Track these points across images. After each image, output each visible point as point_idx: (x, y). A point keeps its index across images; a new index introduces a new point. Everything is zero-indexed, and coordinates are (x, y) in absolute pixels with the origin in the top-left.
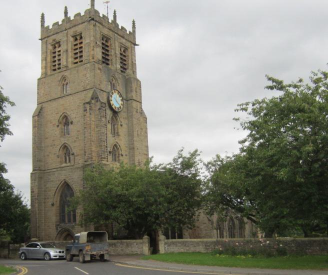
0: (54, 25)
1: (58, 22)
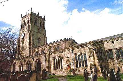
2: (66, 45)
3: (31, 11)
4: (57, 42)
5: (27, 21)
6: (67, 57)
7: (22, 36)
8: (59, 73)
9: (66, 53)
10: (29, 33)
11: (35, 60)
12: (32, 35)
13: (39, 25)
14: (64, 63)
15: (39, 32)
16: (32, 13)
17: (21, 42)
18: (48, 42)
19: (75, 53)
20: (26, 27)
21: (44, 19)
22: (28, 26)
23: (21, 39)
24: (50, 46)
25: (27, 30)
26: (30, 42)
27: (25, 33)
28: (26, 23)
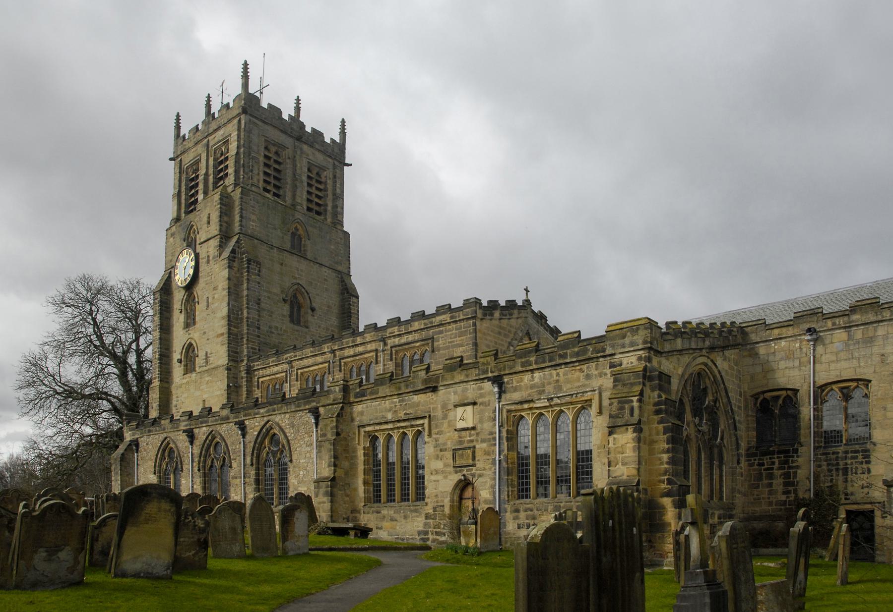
2: (476, 344)
3: (245, 85)
4: (416, 325)
5: (215, 167)
6: (458, 429)
7: (182, 276)
8: (397, 525)
9: (454, 399)
10: (226, 253)
11: (252, 433)
12: (242, 262)
13: (302, 197)
14: (439, 465)
15: (297, 247)
16: (249, 104)
17: (178, 319)
18: (363, 322)
19: (516, 396)
20: (209, 209)
21: (336, 153)
22: (217, 197)
23: (178, 296)
24: (369, 347)
25: (214, 229)
26: (233, 319)
27: (202, 251)
28: (211, 179)
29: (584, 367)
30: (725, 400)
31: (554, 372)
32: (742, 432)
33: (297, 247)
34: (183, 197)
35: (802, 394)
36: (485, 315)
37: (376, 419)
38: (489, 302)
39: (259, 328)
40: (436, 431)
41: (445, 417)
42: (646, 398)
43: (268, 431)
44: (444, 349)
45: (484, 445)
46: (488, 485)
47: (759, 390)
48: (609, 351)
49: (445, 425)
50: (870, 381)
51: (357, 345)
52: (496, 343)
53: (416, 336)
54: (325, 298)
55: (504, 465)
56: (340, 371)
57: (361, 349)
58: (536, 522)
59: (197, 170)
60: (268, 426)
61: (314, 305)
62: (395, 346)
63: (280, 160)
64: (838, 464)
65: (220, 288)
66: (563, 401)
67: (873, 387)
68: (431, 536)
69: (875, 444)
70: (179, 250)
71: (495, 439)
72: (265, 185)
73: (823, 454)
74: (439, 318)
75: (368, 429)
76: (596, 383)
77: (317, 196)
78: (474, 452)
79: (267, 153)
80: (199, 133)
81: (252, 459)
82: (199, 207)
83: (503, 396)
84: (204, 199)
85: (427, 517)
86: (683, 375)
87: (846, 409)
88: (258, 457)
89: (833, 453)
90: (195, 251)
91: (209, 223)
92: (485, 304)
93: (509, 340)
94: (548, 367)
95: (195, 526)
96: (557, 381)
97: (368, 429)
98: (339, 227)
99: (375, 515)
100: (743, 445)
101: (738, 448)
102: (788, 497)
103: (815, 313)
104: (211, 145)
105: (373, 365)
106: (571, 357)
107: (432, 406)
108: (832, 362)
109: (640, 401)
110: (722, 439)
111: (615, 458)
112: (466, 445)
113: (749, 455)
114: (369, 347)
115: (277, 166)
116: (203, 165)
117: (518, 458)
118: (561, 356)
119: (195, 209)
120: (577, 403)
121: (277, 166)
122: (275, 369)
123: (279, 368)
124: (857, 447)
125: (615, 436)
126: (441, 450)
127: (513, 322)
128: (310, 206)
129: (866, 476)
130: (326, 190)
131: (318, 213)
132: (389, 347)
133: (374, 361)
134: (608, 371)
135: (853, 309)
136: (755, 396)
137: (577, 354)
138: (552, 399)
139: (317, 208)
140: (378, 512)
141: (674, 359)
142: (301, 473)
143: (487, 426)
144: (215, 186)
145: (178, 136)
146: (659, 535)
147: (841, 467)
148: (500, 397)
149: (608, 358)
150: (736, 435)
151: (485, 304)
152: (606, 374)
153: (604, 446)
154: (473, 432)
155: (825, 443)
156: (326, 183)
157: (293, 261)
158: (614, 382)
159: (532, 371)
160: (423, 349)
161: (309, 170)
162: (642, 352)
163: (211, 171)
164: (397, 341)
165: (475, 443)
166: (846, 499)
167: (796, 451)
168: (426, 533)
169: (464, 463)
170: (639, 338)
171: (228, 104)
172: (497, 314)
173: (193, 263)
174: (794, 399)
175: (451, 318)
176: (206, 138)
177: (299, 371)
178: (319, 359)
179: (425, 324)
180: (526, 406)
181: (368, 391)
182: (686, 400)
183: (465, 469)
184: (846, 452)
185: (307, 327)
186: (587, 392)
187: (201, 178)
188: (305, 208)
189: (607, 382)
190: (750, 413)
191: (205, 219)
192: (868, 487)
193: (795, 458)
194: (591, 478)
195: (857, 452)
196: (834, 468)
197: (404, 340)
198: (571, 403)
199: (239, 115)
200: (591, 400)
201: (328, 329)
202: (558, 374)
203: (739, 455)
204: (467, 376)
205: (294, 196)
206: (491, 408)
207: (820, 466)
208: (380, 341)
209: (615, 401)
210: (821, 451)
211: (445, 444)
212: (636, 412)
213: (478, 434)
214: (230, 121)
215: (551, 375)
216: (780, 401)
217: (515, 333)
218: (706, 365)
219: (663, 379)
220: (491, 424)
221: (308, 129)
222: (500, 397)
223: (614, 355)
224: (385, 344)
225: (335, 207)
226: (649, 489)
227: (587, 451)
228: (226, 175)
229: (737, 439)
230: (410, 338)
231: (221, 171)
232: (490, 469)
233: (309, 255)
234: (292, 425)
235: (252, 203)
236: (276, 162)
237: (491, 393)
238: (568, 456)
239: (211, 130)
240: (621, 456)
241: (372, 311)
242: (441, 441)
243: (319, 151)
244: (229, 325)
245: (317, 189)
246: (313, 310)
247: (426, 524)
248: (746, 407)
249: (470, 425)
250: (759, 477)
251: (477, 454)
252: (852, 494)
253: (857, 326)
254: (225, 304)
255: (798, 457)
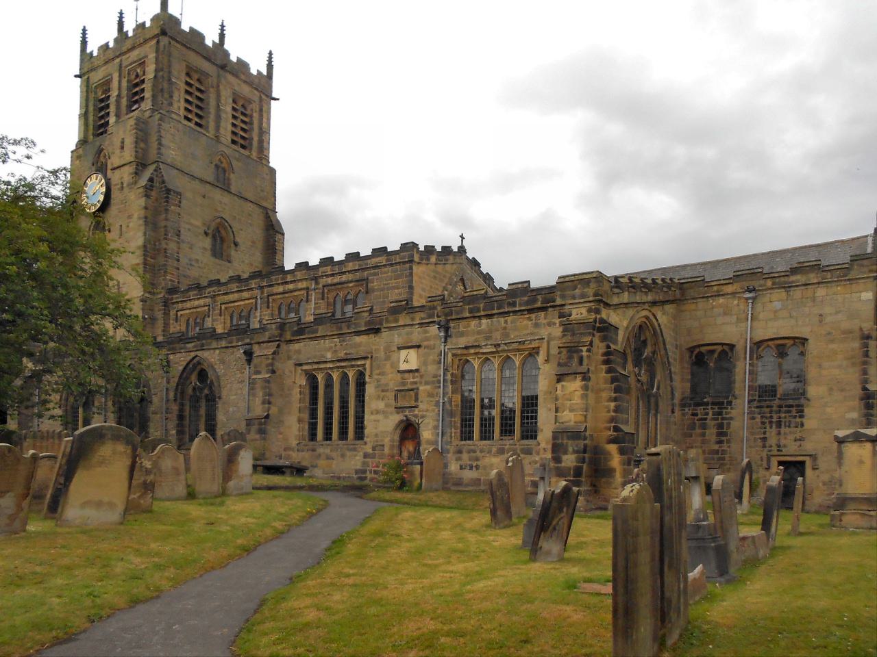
0: (101, 48)
1: (107, 44)
5: (129, 89)
10: (143, 181)
14: (381, 405)
15: (222, 180)
19: (463, 341)
21: (263, 86)
22: (132, 122)
24: (300, 285)
25: (128, 155)
28: (124, 102)
29: (533, 316)
30: (663, 352)
31: (502, 320)
32: (677, 383)
33: (222, 180)
34: (91, 118)
35: (739, 347)
36: (422, 259)
37: (315, 358)
38: (426, 247)
39: (178, 260)
40: (378, 372)
41: (388, 358)
42: (594, 349)
43: (195, 366)
44: (378, 290)
45: (428, 387)
46: (430, 427)
47: (695, 344)
48: (559, 302)
49: (388, 366)
50: (807, 340)
51: (287, 283)
52: (431, 287)
53: (350, 277)
54: (249, 234)
55: (448, 406)
56: (268, 307)
57: (291, 286)
58: (479, 463)
59: (109, 90)
60: (195, 361)
61: (238, 239)
62: (328, 286)
63: (203, 88)
64: (771, 417)
65: (136, 216)
66: (511, 348)
67: (812, 346)
68: (369, 475)
69: (808, 400)
70: (87, 173)
71: (439, 382)
72: (186, 113)
73: (757, 407)
74: (374, 260)
75: (305, 367)
76: (544, 332)
77: (242, 129)
78: (417, 395)
79: (188, 80)
80: (110, 52)
81: (176, 394)
82: (110, 129)
83: (449, 340)
84: (116, 122)
85: (366, 456)
86: (627, 328)
87: (780, 365)
88: (183, 393)
89: (767, 407)
90: (105, 177)
91: (122, 148)
92: (422, 248)
93: (444, 285)
94: (497, 314)
95: (142, 467)
96: (505, 328)
97: (305, 367)
98: (264, 162)
99: (310, 452)
100: (678, 395)
101: (673, 399)
102: (720, 447)
103: (753, 274)
104: (123, 65)
105: (302, 304)
106: (521, 305)
107: (374, 347)
108: (770, 320)
109: (589, 351)
110: (658, 388)
111: (563, 404)
112: (409, 387)
113: (683, 405)
114: (300, 285)
115: (198, 94)
116: (115, 84)
117: (462, 401)
118: (510, 304)
119: (105, 132)
120: (524, 350)
121: (198, 94)
122: (196, 303)
123: (201, 302)
124: (791, 402)
125: (563, 383)
126: (383, 391)
127: (448, 267)
128: (235, 139)
129: (799, 429)
130: (251, 123)
131: (243, 147)
132: (321, 286)
133: (254, 308)
134: (557, 321)
135: (794, 271)
136: (691, 350)
137: (527, 303)
138: (499, 345)
139: (242, 142)
140: (314, 450)
141: (619, 311)
142: (231, 409)
143: (432, 369)
144: (130, 109)
145: (85, 56)
146: (604, 480)
147: (774, 420)
148: (446, 342)
149: (558, 308)
150: (671, 386)
151: (422, 248)
152: (555, 324)
153: (552, 392)
154: (416, 374)
155: (759, 397)
156: (251, 117)
157: (217, 195)
158: (564, 331)
159: (480, 317)
160: (357, 289)
161: (234, 101)
162: (592, 304)
163: (124, 92)
164: (329, 280)
165: (418, 385)
166: (778, 451)
167: (730, 403)
168: (364, 472)
169: (407, 404)
170: (590, 291)
171: (144, 24)
172: (433, 259)
173: (104, 189)
174: (730, 354)
175: (387, 260)
176: (118, 57)
177: (223, 307)
178: (245, 295)
179: (360, 265)
180: (472, 351)
181: (307, 330)
182: (628, 351)
183: (407, 410)
184: (780, 406)
185: (229, 262)
186: (535, 340)
187: (113, 100)
188: (230, 140)
189: (557, 331)
190: (686, 365)
191: (119, 144)
192: (800, 440)
193: (729, 410)
194: (536, 423)
195: (791, 406)
196: (767, 421)
197: (337, 279)
198: (518, 350)
199: (156, 36)
200: (539, 347)
201: (252, 265)
202: (506, 322)
203: (673, 405)
204: (413, 319)
205: (218, 128)
206: (436, 351)
207: (753, 418)
208: (312, 280)
209: (564, 351)
210: (755, 404)
211: (387, 385)
212: (585, 361)
213: (421, 377)
214: (146, 41)
215: (499, 321)
216: (716, 355)
217: (450, 278)
218: (647, 318)
219: (605, 329)
220: (435, 367)
221: (233, 58)
222: (446, 342)
223: (564, 305)
224: (317, 283)
225: (261, 142)
226: (595, 435)
227: (532, 397)
228: (143, 99)
229: (672, 389)
230: (344, 278)
231: (136, 93)
232: (433, 410)
233: (233, 189)
234: (222, 362)
235: (172, 130)
236: (198, 90)
237: (437, 337)
238: (513, 400)
239: (124, 49)
240: (569, 402)
241: (299, 251)
242: (383, 382)
243: (245, 82)
244: (144, 255)
245: (243, 121)
246: (236, 244)
247: (364, 463)
248: (682, 359)
249: (414, 367)
250: (693, 427)
251: (420, 396)
252: (785, 446)
253: (797, 286)
254: (140, 234)
255: (732, 408)
